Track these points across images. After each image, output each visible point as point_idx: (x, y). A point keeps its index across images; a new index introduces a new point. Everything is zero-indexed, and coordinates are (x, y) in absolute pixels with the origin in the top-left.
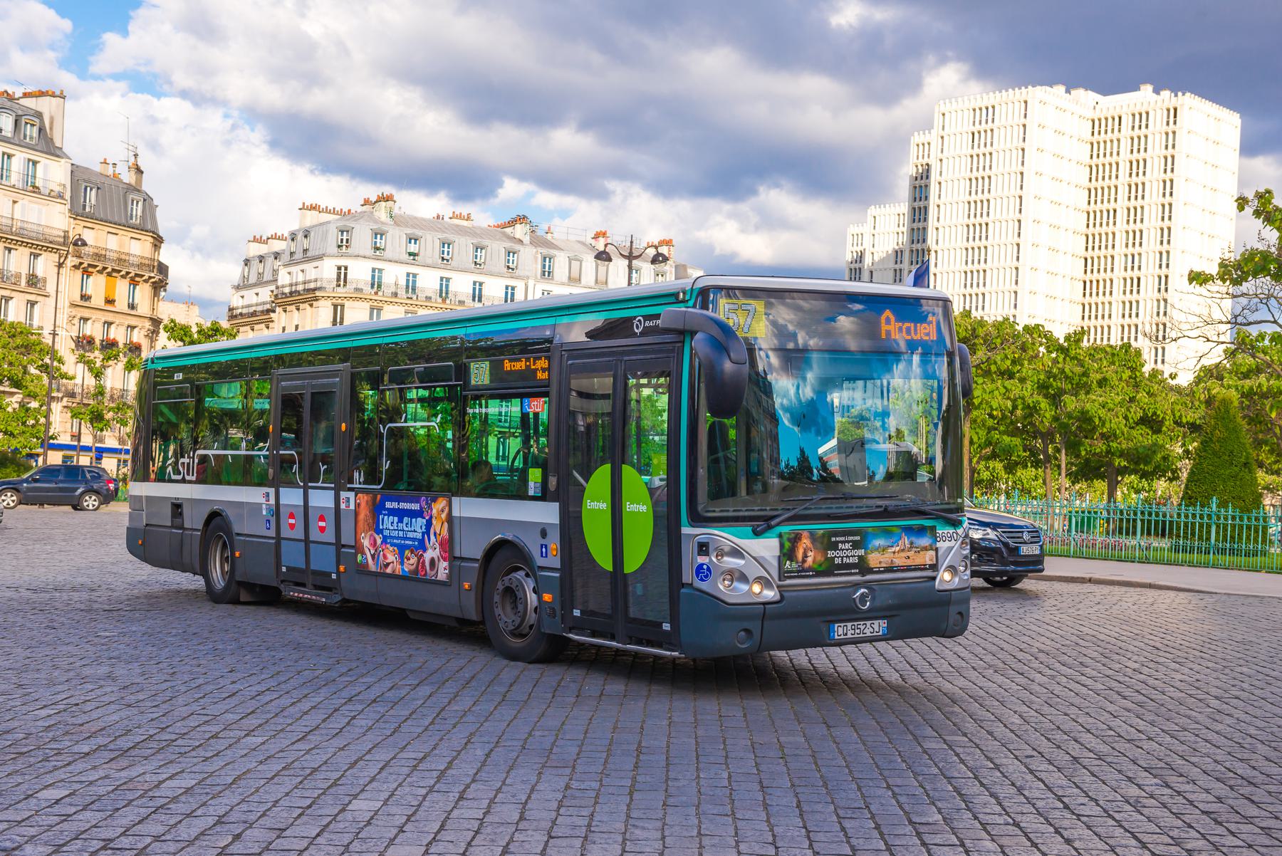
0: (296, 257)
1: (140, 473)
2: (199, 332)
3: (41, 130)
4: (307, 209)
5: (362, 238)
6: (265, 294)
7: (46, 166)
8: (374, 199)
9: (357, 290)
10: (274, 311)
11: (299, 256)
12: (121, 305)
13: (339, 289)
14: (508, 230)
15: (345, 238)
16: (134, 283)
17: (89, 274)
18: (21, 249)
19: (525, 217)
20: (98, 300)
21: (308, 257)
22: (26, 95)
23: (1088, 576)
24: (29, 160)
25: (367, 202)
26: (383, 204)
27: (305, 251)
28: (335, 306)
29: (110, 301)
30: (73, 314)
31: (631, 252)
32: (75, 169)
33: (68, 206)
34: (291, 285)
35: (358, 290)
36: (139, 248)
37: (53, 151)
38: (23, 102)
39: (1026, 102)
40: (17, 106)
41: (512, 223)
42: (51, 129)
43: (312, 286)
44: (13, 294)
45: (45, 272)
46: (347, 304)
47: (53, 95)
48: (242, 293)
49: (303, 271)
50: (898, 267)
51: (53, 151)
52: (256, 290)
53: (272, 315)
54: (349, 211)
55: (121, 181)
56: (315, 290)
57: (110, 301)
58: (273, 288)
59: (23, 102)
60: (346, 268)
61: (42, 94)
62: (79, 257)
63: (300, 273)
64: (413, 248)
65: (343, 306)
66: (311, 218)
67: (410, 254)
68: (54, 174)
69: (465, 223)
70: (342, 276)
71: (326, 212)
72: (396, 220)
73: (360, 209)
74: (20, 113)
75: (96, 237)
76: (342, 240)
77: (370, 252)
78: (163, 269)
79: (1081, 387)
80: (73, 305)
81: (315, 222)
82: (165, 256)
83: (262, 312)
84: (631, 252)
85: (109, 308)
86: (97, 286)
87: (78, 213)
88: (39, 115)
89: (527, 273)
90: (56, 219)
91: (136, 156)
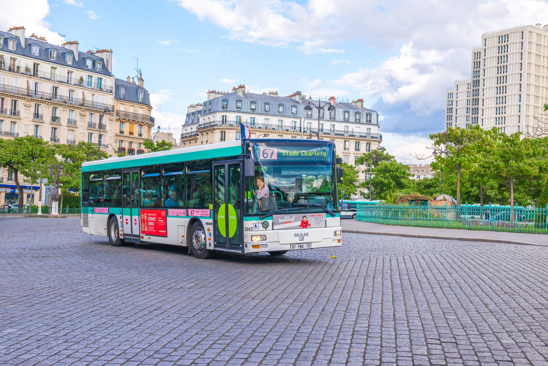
0: (206, 112)
1: (7, 196)
2: (157, 145)
3: (103, 66)
4: (211, 93)
5: (232, 104)
6: (194, 128)
7: (105, 80)
8: (237, 87)
9: (230, 125)
10: (198, 135)
11: (207, 112)
12: (136, 135)
13: (223, 125)
14: (293, 98)
15: (225, 104)
16: (141, 126)
17: (123, 123)
18: (96, 113)
19: (300, 92)
20: (126, 133)
21: (210, 112)
22: (97, 52)
23: (483, 238)
24: (98, 78)
25: (234, 89)
26: (241, 89)
27: (210, 110)
28: (222, 132)
29: (131, 133)
30: (117, 139)
31: (319, 106)
32: (117, 80)
33: (114, 96)
34: (204, 124)
35: (231, 125)
36: (141, 111)
37: (109, 74)
38: (96, 55)
39: (523, 32)
40: (94, 56)
41: (294, 95)
42: (107, 65)
43: (212, 124)
44: (93, 132)
45: (105, 122)
46: (227, 131)
47: (108, 52)
48: (186, 128)
49: (209, 118)
50: (468, 107)
51: (109, 74)
52: (191, 127)
53: (198, 137)
54: (228, 92)
55: (136, 85)
56: (213, 126)
57: (131, 133)
58: (197, 125)
59: (96, 55)
60: (226, 116)
61: (103, 51)
62: (119, 116)
63: (208, 119)
64: (253, 107)
65: (225, 132)
66: (213, 96)
67: (252, 109)
68: (108, 83)
69: (275, 96)
70: (224, 120)
71: (218, 94)
72: (246, 95)
73: (232, 92)
74: (95, 59)
75: (122, 107)
76: (224, 105)
77: (235, 109)
78: (152, 120)
79: (518, 157)
80: (117, 135)
81: (214, 98)
82: (154, 114)
83: (194, 135)
84: (319, 106)
85: (131, 136)
86: (126, 127)
87: (117, 98)
88: (102, 60)
89: (301, 116)
90: (108, 100)
91: (141, 74)
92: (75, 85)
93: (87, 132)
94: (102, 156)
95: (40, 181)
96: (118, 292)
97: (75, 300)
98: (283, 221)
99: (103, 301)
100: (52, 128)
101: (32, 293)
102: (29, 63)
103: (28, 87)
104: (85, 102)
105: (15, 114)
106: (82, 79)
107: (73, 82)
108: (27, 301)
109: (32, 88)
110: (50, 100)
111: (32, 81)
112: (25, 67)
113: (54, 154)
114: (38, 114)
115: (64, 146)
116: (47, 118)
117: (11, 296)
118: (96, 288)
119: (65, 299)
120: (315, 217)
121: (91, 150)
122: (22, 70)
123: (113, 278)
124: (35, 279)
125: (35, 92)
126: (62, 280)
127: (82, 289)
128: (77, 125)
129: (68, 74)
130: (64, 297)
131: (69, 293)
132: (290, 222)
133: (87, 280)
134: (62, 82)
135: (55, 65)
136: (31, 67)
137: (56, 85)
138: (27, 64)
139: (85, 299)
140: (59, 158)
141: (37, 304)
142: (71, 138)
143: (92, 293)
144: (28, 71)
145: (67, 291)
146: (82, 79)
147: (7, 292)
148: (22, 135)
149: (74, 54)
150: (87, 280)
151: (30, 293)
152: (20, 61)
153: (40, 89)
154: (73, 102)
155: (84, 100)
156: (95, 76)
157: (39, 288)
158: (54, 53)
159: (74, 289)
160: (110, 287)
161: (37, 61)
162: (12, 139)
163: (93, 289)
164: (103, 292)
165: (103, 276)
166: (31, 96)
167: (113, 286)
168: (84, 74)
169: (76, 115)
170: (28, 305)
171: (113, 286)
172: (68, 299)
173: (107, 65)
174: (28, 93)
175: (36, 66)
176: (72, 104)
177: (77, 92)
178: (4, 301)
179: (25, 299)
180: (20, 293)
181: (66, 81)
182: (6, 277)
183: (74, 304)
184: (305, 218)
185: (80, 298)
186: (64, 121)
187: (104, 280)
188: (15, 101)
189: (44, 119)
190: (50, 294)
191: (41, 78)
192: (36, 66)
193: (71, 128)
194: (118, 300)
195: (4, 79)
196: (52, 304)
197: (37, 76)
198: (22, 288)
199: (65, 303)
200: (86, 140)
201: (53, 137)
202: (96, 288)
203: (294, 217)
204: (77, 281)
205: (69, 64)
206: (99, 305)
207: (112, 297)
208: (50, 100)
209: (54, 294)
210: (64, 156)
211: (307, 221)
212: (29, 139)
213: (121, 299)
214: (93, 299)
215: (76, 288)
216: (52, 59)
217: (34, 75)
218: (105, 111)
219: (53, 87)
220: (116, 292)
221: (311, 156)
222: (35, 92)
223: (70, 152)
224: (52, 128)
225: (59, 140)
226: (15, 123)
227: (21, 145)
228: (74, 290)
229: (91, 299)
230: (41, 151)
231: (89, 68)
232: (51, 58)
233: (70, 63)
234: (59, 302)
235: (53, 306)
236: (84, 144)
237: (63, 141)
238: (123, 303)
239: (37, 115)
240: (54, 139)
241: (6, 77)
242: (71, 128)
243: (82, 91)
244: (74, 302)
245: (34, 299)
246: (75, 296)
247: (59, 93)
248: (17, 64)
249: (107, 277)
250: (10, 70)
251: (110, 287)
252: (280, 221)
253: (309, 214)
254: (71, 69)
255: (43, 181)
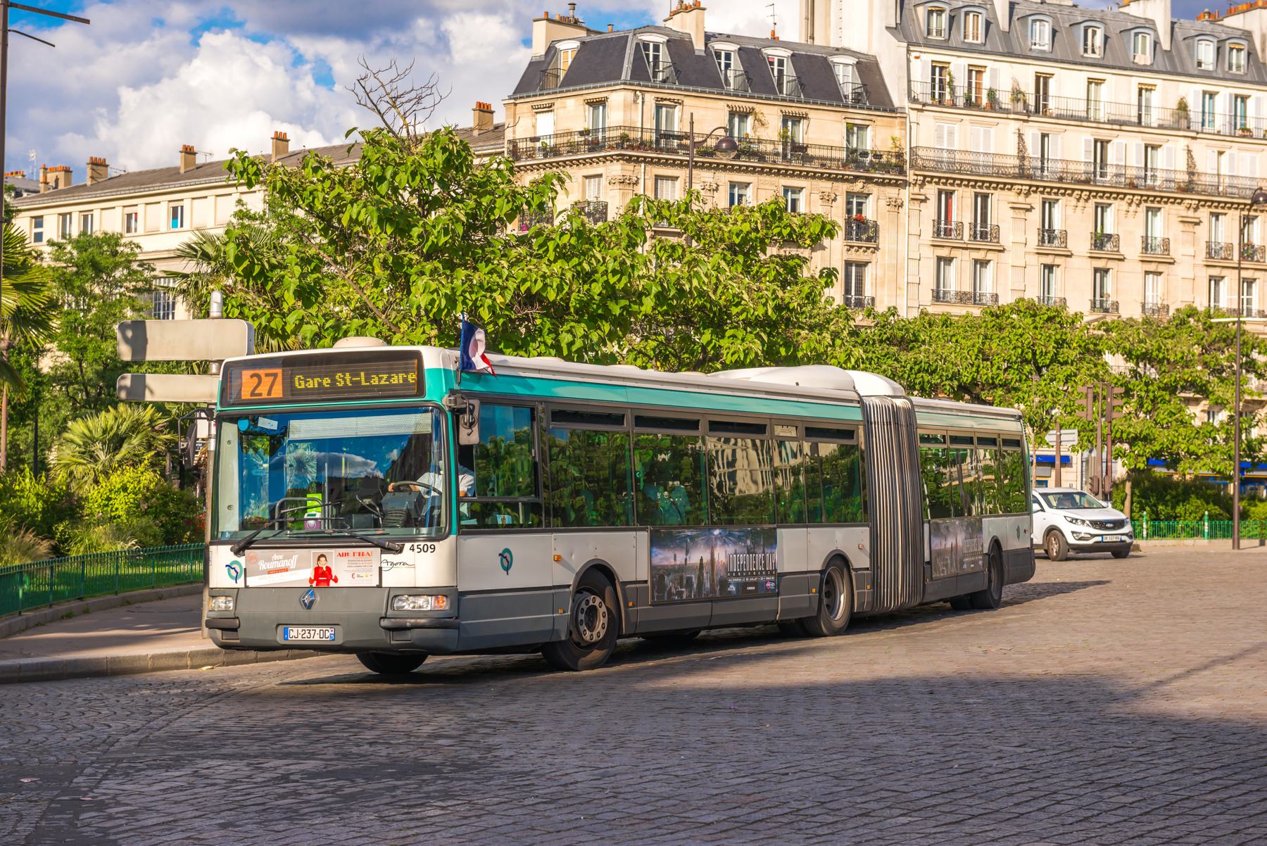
24: (1236, 96)
40: (1220, 29)
92: (1161, 127)
93: (1204, 274)
94: (1253, 347)
95: (1054, 438)
96: (1230, 792)
97: (1089, 814)
98: (271, 566)
99: (1175, 821)
100: (1096, 270)
101: (967, 783)
102: (1022, 75)
103: (1020, 151)
104: (1195, 178)
105: (984, 235)
106: (1183, 107)
107: (1155, 117)
108: (947, 808)
109: (1033, 151)
110: (1087, 182)
111: (1032, 132)
112: (1010, 89)
113: (1100, 353)
114: (1051, 231)
115: (1130, 323)
116: (1080, 243)
117: (905, 789)
118: (1165, 778)
119: (1058, 808)
120: (351, 558)
121: (1214, 333)
122: (1005, 99)
123: (1229, 747)
124: (986, 742)
125: (1043, 163)
126: (1066, 748)
127: (1119, 780)
128: (1172, 254)
129: (1140, 94)
130: (1058, 803)
131: (1076, 791)
132: (286, 570)
133: (1143, 752)
134: (1122, 123)
135: (1097, 73)
136: (1029, 88)
137: (1103, 135)
138: (1015, 81)
139: (1119, 812)
140: (1116, 363)
141: (973, 817)
142: (1153, 299)
143: (1146, 794)
144: (1018, 100)
145: (1071, 784)
146: (1183, 107)
147: (899, 776)
148: (1006, 299)
149: (1155, 30)
150: (1143, 752)
151: (960, 784)
152: (994, 73)
153: (1054, 152)
154: (1158, 183)
155: (1191, 174)
156: (1225, 93)
157: (990, 770)
158: (1094, 33)
159: (1095, 777)
160: (1208, 776)
161: (1045, 68)
162: (976, 311)
163: (1152, 780)
164: (1182, 792)
165: (1197, 742)
166: (1029, 177)
167: (1218, 773)
168: (1191, 91)
169: (1165, 224)
170: (950, 818)
171: (1218, 773)
172: (1070, 808)
173: (1263, 50)
174: (1021, 167)
175: (1042, 82)
176: (1153, 189)
177: (1169, 149)
178: (882, 805)
179: (941, 801)
180: (933, 783)
181: (1135, 120)
182: (909, 731)
183: (1086, 825)
184: (322, 559)
185: (1104, 807)
186: (1131, 248)
187: (1196, 754)
188: (985, 197)
189: (1072, 245)
190: (1018, 788)
191: (1059, 117)
192: (1042, 82)
193: (1152, 267)
194: (1222, 820)
195: (951, 133)
196: (1019, 821)
197: (1045, 114)
198: (944, 766)
199: (1057, 821)
200: (1201, 304)
201: (1098, 297)
202: (1165, 778)
203: (295, 557)
204: (1110, 751)
205: (1142, 63)
206: (1159, 833)
207: (1208, 809)
208: (1087, 182)
209: (1031, 789)
210: (1129, 355)
211: (329, 569)
212: (1031, 310)
213: (1234, 817)
214: (1146, 813)
215: (1099, 776)
216: (1090, 55)
217: (1037, 111)
218: (1255, 201)
219: (1096, 141)
220: (1223, 795)
221: (399, 385)
222: (1043, 163)
223: (1150, 345)
224: (1096, 270)
225: (1116, 306)
226: (984, 263)
227: (1001, 329)
228: (1093, 782)
229: (1138, 812)
230: (1060, 344)
231: (1203, 67)
232: (1086, 51)
233: (1144, 59)
234: (1042, 815)
235: (1019, 826)
236: (1192, 312)
237: (1130, 310)
238: (1238, 832)
239: (1047, 234)
240: (1100, 303)
241: (957, 127)
242: (1152, 267)
243: (1183, 143)
244: (1086, 819)
245: (968, 801)
246: (1090, 800)
247: (1112, 157)
248: (986, 83)
249: (1210, 744)
250: (969, 104)
251: (1208, 776)
252: (263, 565)
253: (333, 550)
254: (1147, 79)
255: (1063, 438)
